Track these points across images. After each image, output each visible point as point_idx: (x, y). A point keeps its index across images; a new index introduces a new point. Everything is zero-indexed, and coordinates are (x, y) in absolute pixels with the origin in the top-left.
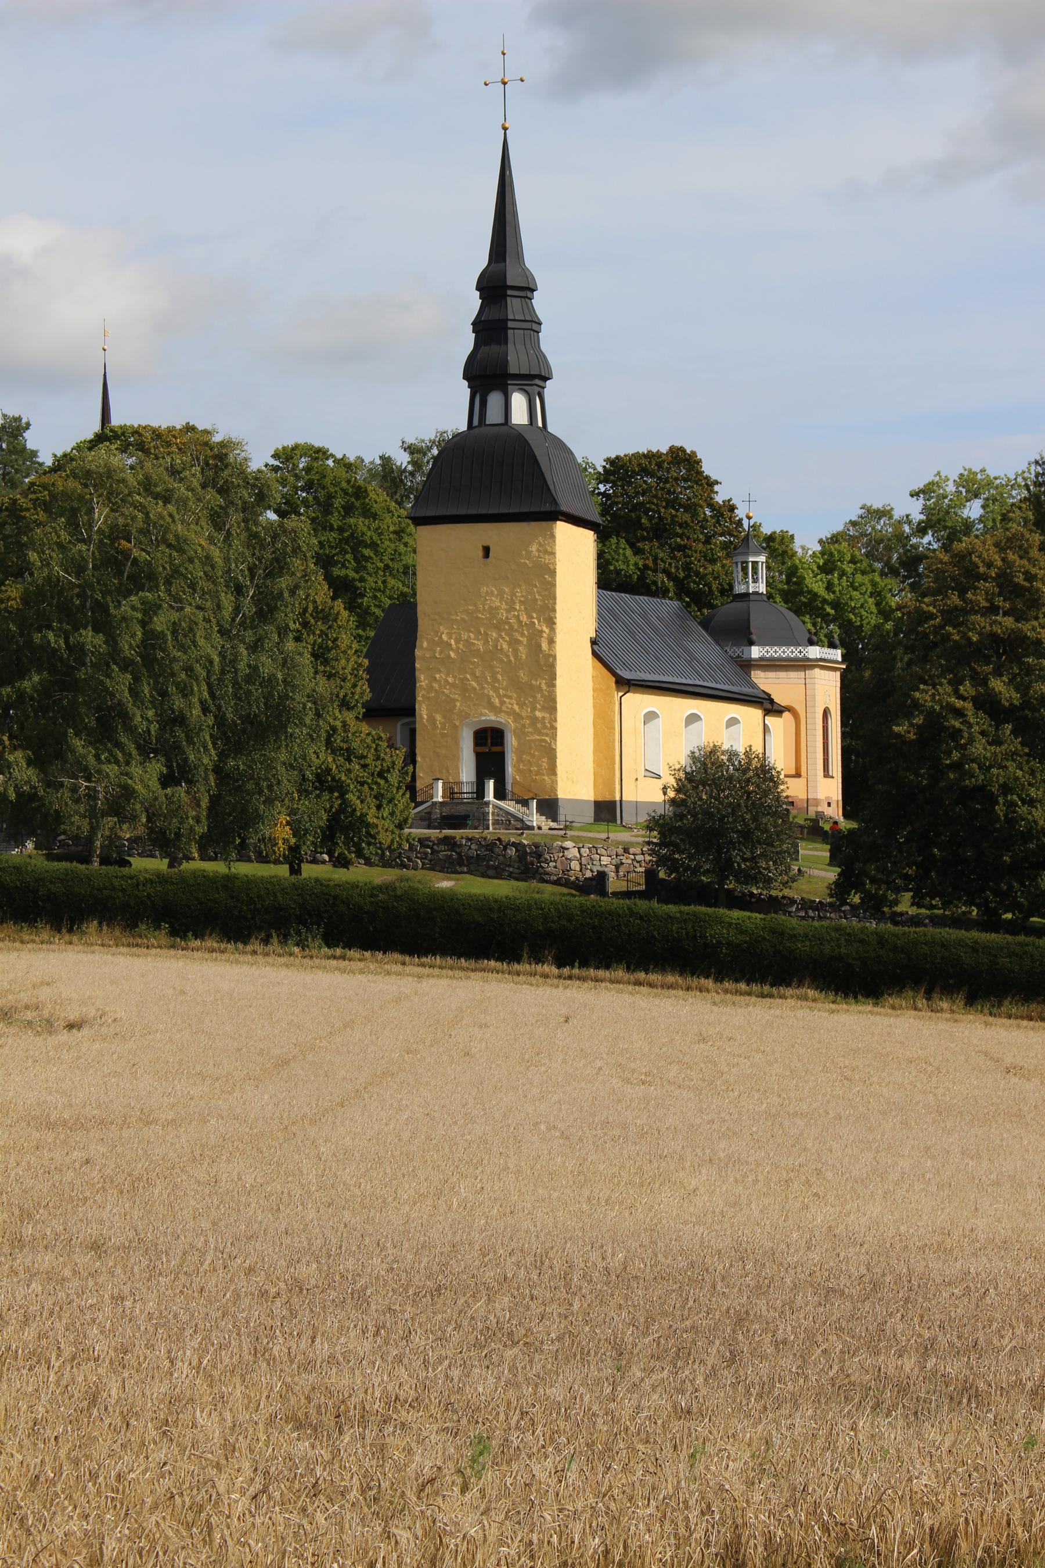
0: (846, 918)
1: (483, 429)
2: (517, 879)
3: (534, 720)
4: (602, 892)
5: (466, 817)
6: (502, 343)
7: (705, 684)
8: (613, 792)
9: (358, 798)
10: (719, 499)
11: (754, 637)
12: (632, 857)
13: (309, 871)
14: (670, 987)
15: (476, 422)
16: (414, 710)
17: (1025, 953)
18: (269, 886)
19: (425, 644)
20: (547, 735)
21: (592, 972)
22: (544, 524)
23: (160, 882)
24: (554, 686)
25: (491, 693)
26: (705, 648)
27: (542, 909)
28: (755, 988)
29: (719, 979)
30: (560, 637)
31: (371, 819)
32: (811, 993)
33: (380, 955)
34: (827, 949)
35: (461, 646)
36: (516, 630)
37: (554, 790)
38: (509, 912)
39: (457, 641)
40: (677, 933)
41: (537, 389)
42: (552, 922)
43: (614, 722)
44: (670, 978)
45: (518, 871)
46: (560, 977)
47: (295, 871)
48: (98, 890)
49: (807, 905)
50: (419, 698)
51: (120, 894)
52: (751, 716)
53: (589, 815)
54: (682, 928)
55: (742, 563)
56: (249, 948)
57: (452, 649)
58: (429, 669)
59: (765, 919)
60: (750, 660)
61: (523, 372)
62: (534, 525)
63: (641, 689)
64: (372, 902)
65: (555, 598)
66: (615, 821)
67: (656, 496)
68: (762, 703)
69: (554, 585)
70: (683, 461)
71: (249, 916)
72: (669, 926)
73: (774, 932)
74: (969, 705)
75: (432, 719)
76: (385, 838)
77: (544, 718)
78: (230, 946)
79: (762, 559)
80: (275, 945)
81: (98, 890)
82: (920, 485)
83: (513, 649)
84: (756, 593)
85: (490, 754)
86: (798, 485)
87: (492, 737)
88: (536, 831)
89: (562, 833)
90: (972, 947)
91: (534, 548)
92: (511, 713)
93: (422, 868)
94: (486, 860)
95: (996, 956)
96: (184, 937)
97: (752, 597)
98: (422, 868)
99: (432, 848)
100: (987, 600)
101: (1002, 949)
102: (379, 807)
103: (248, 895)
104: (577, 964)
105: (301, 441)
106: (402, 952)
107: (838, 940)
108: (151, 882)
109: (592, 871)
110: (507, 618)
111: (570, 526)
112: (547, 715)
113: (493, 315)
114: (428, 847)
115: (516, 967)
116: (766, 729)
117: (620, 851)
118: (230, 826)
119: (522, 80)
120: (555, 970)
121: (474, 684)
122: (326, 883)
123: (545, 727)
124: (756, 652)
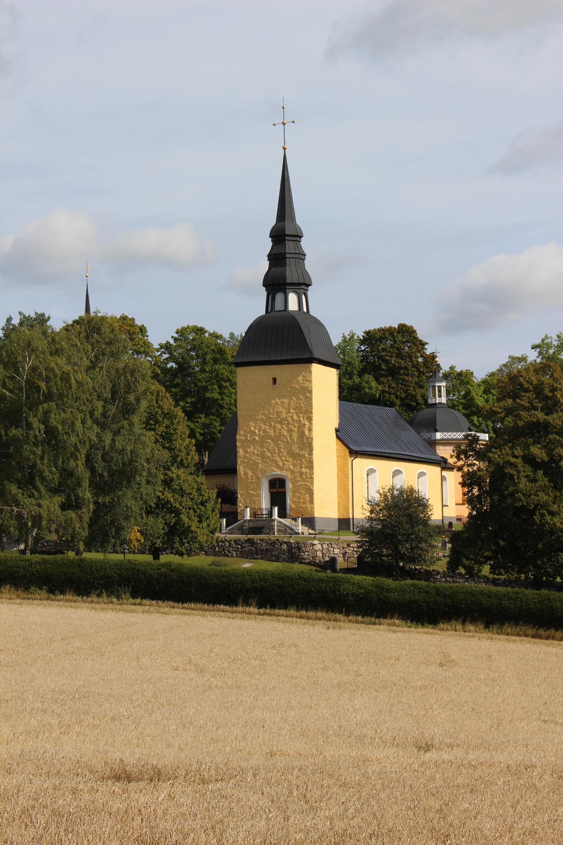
0: (468, 582)
1: (273, 314)
2: (287, 562)
3: (301, 474)
4: (334, 570)
5: (263, 528)
7: (405, 453)
8: (348, 513)
9: (187, 517)
10: (428, 352)
11: (438, 427)
12: (352, 549)
13: (164, 558)
14: (320, 619)
15: (269, 310)
16: (236, 469)
17: (518, 598)
18: (102, 564)
19: (242, 432)
20: (308, 482)
21: (277, 611)
22: (306, 365)
23: (44, 563)
24: (312, 454)
25: (278, 459)
26: (410, 434)
27: (251, 576)
28: (366, 619)
29: (347, 614)
30: (315, 427)
31: (193, 529)
32: (397, 622)
33: (160, 603)
34: (407, 597)
35: (261, 433)
36: (291, 424)
37: (312, 512)
38: (233, 578)
39: (259, 431)
40: (325, 588)
41: (303, 291)
43: (348, 474)
44: (320, 614)
45: (288, 558)
46: (259, 614)
48: (10, 568)
50: (239, 463)
51: (22, 570)
52: (434, 471)
53: (335, 527)
54: (327, 586)
55: (433, 386)
56: (89, 599)
57: (256, 435)
58: (244, 446)
59: (373, 580)
60: (436, 440)
61: (294, 282)
62: (300, 366)
63: (371, 457)
65: (312, 406)
66: (349, 529)
68: (440, 464)
69: (311, 399)
70: (406, 331)
71: (91, 582)
72: (320, 584)
73: (378, 588)
74: (519, 461)
75: (246, 474)
76: (202, 538)
78: (79, 598)
79: (444, 384)
80: (105, 598)
81: (10, 568)
82: (538, 341)
84: (440, 403)
85: (278, 493)
87: (279, 484)
88: (301, 535)
89: (313, 536)
90: (488, 595)
91: (300, 379)
92: (289, 470)
93: (236, 556)
94: (270, 552)
95: (501, 600)
96: (54, 594)
97: (438, 406)
98: (236, 556)
99: (241, 545)
100: (529, 402)
101: (504, 596)
102: (200, 521)
103: (91, 570)
104: (268, 607)
105: (191, 324)
106: (175, 601)
107: (414, 591)
108: (39, 563)
109: (329, 557)
110: (286, 417)
111: (321, 366)
112: (308, 471)
113: (278, 251)
114: (239, 544)
115: (235, 608)
116: (443, 478)
117: (345, 545)
118: (102, 532)
119: (293, 122)
120: (256, 610)
122: (134, 563)
123: (307, 478)
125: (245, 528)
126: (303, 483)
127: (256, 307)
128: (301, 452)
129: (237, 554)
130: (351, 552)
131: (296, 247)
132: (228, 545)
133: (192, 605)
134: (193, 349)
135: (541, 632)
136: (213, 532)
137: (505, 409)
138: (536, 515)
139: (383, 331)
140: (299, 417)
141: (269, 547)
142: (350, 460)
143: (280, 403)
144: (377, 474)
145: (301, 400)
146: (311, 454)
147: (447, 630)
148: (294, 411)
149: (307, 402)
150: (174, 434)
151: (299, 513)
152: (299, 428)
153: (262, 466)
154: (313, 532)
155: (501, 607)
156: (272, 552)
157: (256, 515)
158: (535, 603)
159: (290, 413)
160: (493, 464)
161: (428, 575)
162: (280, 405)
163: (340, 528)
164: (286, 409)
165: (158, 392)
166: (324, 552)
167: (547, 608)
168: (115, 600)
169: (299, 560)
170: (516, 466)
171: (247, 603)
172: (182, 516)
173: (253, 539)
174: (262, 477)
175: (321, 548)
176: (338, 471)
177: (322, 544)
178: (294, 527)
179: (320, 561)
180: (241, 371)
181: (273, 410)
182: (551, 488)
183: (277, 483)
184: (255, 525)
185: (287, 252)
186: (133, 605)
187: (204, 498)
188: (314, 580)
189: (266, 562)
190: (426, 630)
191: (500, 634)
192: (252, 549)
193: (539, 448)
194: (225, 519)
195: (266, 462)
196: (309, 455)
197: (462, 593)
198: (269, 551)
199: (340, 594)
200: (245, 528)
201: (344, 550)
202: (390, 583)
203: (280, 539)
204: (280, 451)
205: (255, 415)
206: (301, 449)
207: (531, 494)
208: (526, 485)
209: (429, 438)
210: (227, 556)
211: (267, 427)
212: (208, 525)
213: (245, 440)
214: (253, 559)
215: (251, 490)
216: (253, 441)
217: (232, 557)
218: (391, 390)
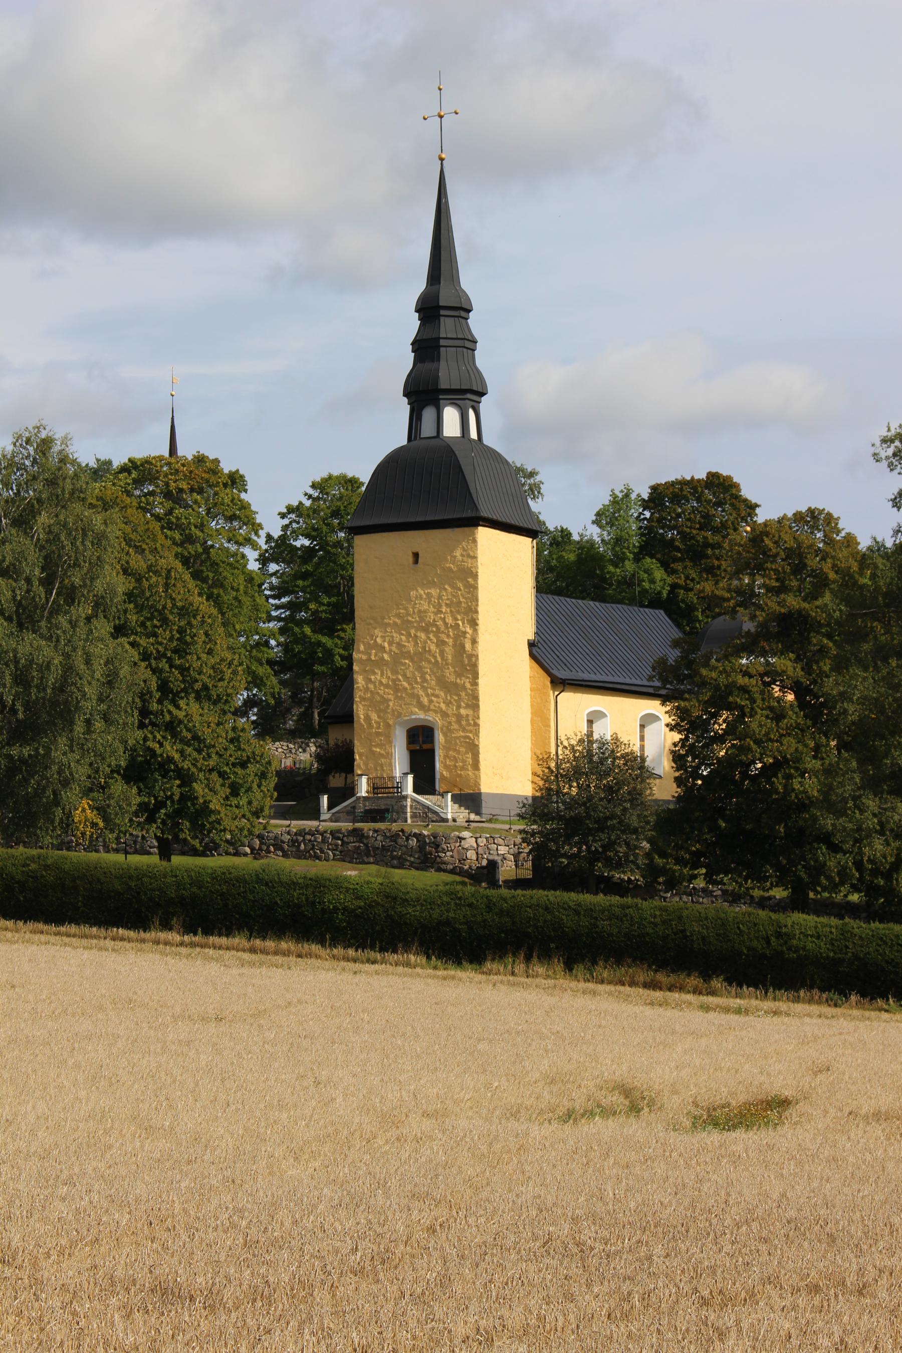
2: (417, 869)
3: (459, 717)
4: (493, 883)
6: (440, 363)
17: (626, 915)
19: (362, 648)
20: (471, 732)
22: (467, 529)
24: (476, 684)
25: (421, 693)
27: (176, 876)
30: (482, 638)
32: (412, 958)
33: (20, 924)
34: (436, 914)
35: (394, 648)
36: (443, 632)
37: (477, 784)
39: (390, 644)
42: (184, 889)
43: (549, 719)
45: (418, 861)
50: (357, 699)
57: (385, 652)
58: (365, 671)
61: (475, 388)
64: (23, 872)
65: (477, 600)
67: (689, 520)
69: (476, 588)
72: (291, 892)
73: (387, 897)
75: (368, 718)
77: (467, 715)
83: (440, 651)
85: (422, 751)
90: (575, 910)
91: (458, 553)
94: (389, 853)
95: (596, 919)
99: (342, 840)
105: (335, 473)
107: (448, 903)
112: (470, 712)
114: (338, 838)
121: (405, 684)
123: (469, 725)
126: (462, 734)
127: (391, 430)
128: (458, 681)
129: (334, 855)
132: (320, 840)
135: (661, 977)
139: (683, 483)
140: (456, 619)
141: (388, 843)
142: (551, 695)
145: (460, 590)
146: (475, 684)
148: (448, 610)
149: (469, 593)
150: (191, 644)
152: (456, 638)
153: (394, 704)
154: (477, 818)
155: (596, 932)
156: (392, 852)
158: (656, 925)
159: (441, 612)
162: (424, 599)
164: (434, 607)
165: (169, 571)
166: (480, 851)
167: (675, 934)
169: (436, 866)
171: (166, 926)
173: (362, 830)
174: (395, 724)
176: (532, 713)
177: (476, 838)
179: (470, 867)
180: (360, 541)
181: (414, 608)
184: (374, 807)
187: (244, 754)
191: (589, 981)
192: (359, 846)
194: (326, 797)
195: (401, 698)
196: (472, 685)
197: (530, 907)
198: (388, 850)
199: (323, 909)
204: (424, 680)
205: (383, 618)
206: (459, 675)
211: (403, 638)
212: (250, 803)
213: (366, 660)
214: (360, 863)
215: (375, 746)
216: (380, 663)
217: (327, 861)
218: (688, 582)
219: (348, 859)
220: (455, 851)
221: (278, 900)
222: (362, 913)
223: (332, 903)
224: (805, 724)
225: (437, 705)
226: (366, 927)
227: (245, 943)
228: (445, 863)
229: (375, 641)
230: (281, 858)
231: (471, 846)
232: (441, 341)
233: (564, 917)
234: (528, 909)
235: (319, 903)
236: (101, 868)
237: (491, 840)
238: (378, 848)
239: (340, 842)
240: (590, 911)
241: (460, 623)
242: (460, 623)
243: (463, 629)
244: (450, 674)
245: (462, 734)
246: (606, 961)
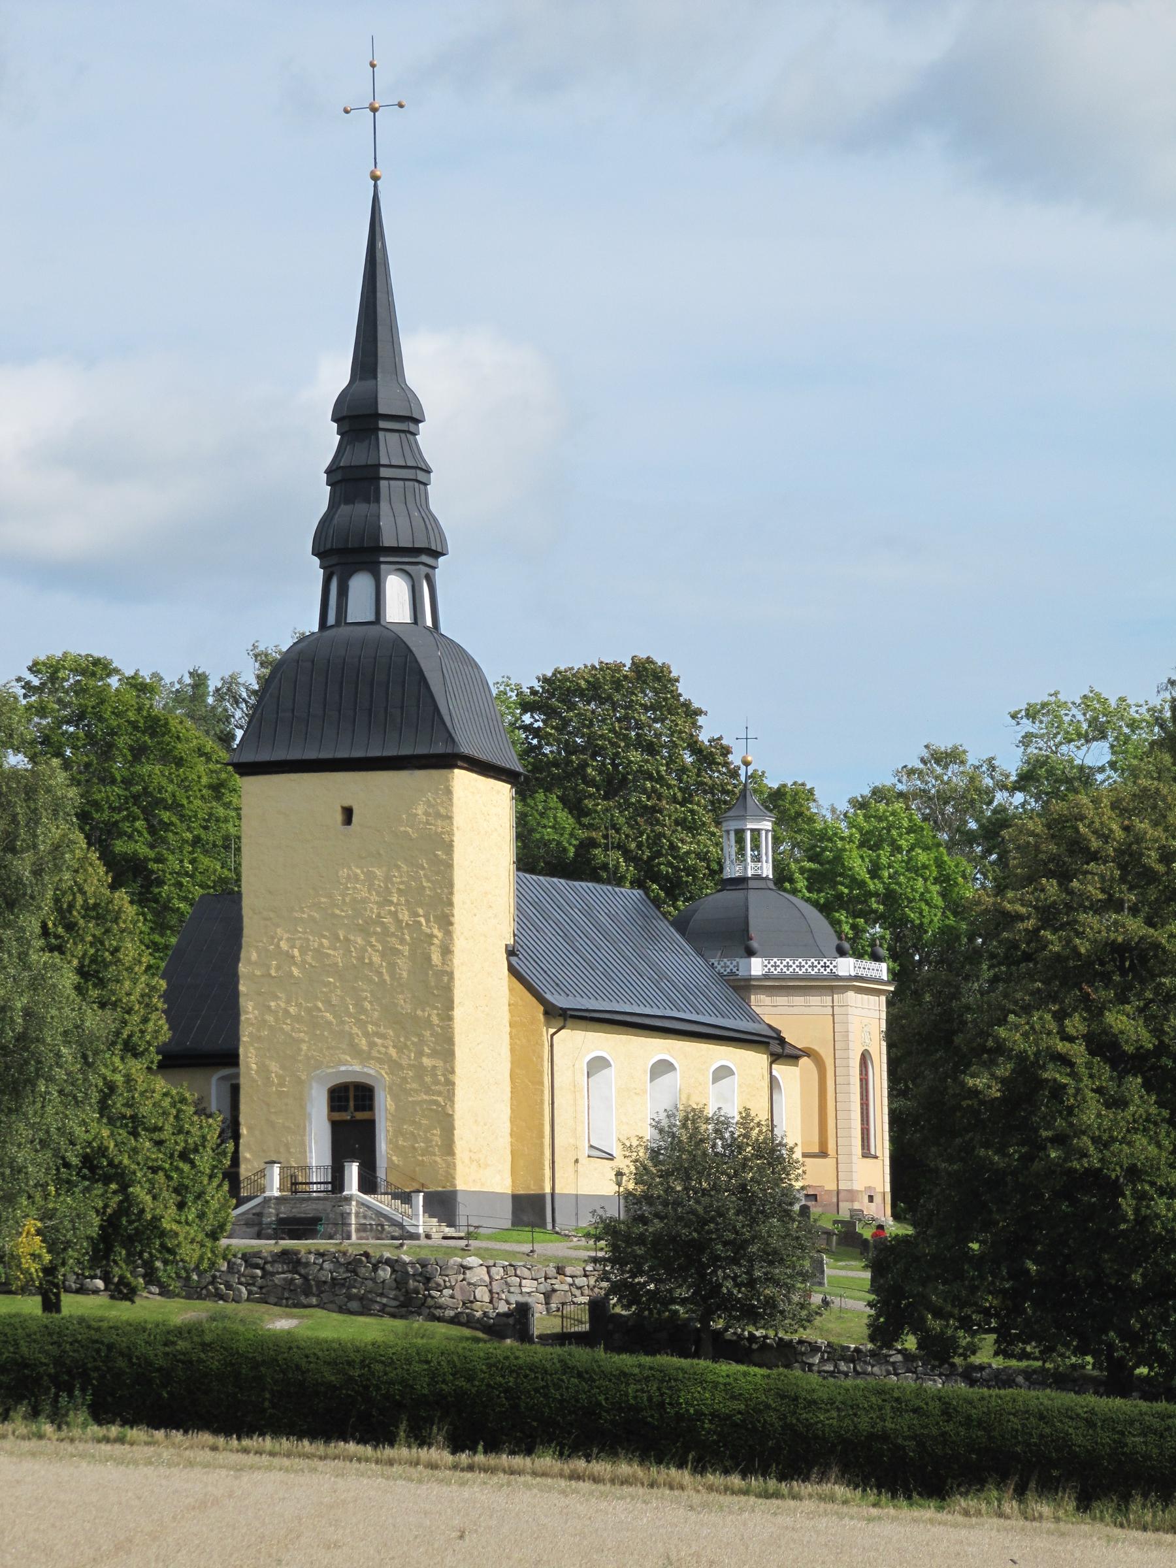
0: (897, 1374)
1: (343, 631)
2: (393, 1316)
3: (420, 1070)
5: (316, 1220)
11: (755, 944)
12: (569, 1280)
14: (625, 1482)
15: (331, 620)
16: (237, 1056)
19: (254, 956)
20: (440, 1094)
21: (505, 1459)
22: (435, 774)
24: (450, 1018)
25: (355, 1030)
26: (679, 960)
27: (427, 1362)
28: (755, 1482)
29: (700, 1468)
30: (460, 944)
31: (166, 1225)
32: (840, 1490)
34: (864, 1423)
35: (309, 959)
36: (393, 935)
37: (450, 1177)
38: (378, 1367)
39: (303, 952)
41: (424, 570)
42: (444, 1381)
44: (624, 1469)
46: (455, 1467)
47: (51, 1305)
49: (835, 1353)
54: (642, 1391)
57: (295, 964)
58: (260, 994)
59: (768, 1376)
60: (749, 979)
63: (597, 1025)
64: (167, 1354)
66: (543, 1225)
69: (450, 866)
70: (650, 675)
73: (783, 1397)
74: (1078, 1051)
75: (263, 1069)
76: (189, 1253)
83: (389, 963)
84: (758, 877)
85: (354, 1123)
86: (823, 715)
88: (423, 1241)
89: (463, 1243)
90: (1086, 1420)
93: (248, 1300)
94: (345, 1288)
95: (1122, 1433)
97: (751, 884)
98: (248, 1300)
99: (263, 1269)
101: (1132, 1423)
102: (181, 1206)
104: (480, 1448)
106: (216, 1432)
109: (508, 1303)
110: (379, 916)
113: (358, 456)
114: (257, 1266)
115: (388, 1452)
116: (773, 1083)
117: (552, 1271)
119: (401, 106)
120: (447, 1457)
123: (437, 1083)
124: (757, 966)
125: (266, 1220)
126: (425, 1097)
127: (291, 612)
128: (419, 1012)
129: (250, 1293)
130: (566, 1288)
131: (406, 448)
132: (224, 1267)
133: (268, 1443)
134: (79, 718)
136: (214, 1236)
137: (1036, 908)
138: (1124, 1196)
141: (341, 1274)
142: (546, 1032)
143: (362, 877)
144: (611, 1073)
145: (423, 868)
147: (979, 1513)
148: (402, 899)
149: (438, 873)
151: (413, 1179)
155: (1123, 1454)
156: (348, 1288)
157: (295, 1184)
159: (391, 903)
160: (1010, 1058)
161: (788, 1353)
163: (519, 1220)
164: (378, 894)
166: (496, 1288)
168: (48, 1429)
170: (1072, 1065)
172: (134, 1190)
173: (297, 1253)
175: (487, 1278)
176: (512, 1063)
177: (488, 1267)
178: (406, 1222)
179: (485, 1314)
180: (252, 789)
181: (344, 895)
182: (1165, 1125)
183: (351, 1094)
185: (382, 462)
186: (99, 1441)
188: (604, 1375)
189: (334, 1315)
190: (916, 1513)
192: (293, 1279)
193: (1128, 1016)
197: (1014, 1415)
200: (266, 1220)
201: (556, 1281)
202: (814, 1386)
203: (370, 1251)
207: (1113, 1140)
208: (1099, 1115)
209: (732, 973)
210: (222, 1297)
212: (201, 1216)
214: (295, 1306)
219: (272, 1299)
220: (457, 1288)
221: (601, 1398)
222: (743, 1421)
223: (692, 1405)
224: (1159, 1114)
225: (383, 1050)
226: (751, 1443)
227: (557, 1465)
228: (440, 1307)
229: (278, 946)
230: (158, 1298)
231: (481, 1280)
232: (382, 470)
233: (1071, 1431)
234: (1011, 1417)
235: (670, 1404)
236: (298, 1347)
237: (511, 1271)
238: (325, 1282)
239: (259, 1272)
240: (1109, 1422)
241: (422, 920)
242: (422, 920)
243: (428, 931)
244: (404, 1004)
245: (425, 1097)
246: (1145, 1496)
